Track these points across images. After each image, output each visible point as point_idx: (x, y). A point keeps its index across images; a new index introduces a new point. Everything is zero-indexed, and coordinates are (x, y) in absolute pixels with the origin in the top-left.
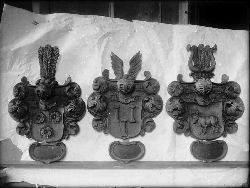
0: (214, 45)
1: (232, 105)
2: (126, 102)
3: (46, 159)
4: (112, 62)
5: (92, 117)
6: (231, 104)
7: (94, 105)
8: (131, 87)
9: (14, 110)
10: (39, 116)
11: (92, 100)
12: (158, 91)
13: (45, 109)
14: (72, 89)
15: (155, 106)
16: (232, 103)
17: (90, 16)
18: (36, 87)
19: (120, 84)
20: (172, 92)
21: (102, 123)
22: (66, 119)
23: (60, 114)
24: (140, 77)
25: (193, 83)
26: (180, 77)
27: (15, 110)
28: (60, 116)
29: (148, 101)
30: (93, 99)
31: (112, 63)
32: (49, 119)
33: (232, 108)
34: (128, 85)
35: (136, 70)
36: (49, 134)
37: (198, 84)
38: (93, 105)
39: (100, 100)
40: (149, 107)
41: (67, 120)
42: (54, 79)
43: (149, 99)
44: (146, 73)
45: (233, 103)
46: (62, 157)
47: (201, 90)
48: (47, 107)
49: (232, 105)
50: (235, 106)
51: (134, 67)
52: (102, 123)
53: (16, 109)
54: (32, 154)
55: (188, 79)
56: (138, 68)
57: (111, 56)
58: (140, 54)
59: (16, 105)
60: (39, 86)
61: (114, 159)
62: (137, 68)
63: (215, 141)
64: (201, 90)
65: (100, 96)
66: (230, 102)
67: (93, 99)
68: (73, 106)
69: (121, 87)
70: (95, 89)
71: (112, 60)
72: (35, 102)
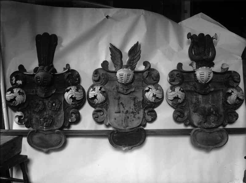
0: (215, 34)
1: (232, 93)
2: (126, 92)
3: (44, 147)
4: (110, 53)
5: (92, 110)
6: (231, 93)
7: (95, 96)
8: (130, 77)
9: (12, 98)
10: (38, 104)
11: (92, 91)
12: (158, 81)
13: (45, 97)
14: (72, 78)
15: (155, 95)
16: (232, 92)
17: (87, 11)
18: (34, 75)
19: (120, 74)
20: (172, 80)
21: (102, 115)
22: (66, 107)
23: (60, 101)
24: (141, 67)
25: (194, 72)
26: (180, 65)
27: (13, 98)
28: (60, 103)
29: (148, 91)
30: (93, 90)
31: (111, 54)
32: (49, 107)
33: (232, 97)
34: (128, 74)
35: (135, 60)
36: (50, 122)
37: (198, 73)
38: (93, 96)
39: (100, 91)
40: (150, 97)
41: (67, 108)
42: (53, 66)
43: (150, 88)
44: (146, 63)
45: (233, 92)
46: (63, 144)
47: (202, 78)
48: (48, 101)
49: (232, 93)
50: (235, 95)
51: (133, 58)
52: (102, 115)
53: (14, 97)
54: (32, 145)
55: (187, 68)
56: (136, 59)
57: (110, 48)
58: (139, 45)
59: (14, 93)
60: (37, 73)
61: (243, 102)
62: (136, 58)
63: (6, 178)
64: (202, 78)
65: (100, 87)
66: (230, 91)
67: (93, 90)
68: (73, 92)
69: (121, 77)
70: (95, 81)
71: (111, 52)
72: (34, 90)
